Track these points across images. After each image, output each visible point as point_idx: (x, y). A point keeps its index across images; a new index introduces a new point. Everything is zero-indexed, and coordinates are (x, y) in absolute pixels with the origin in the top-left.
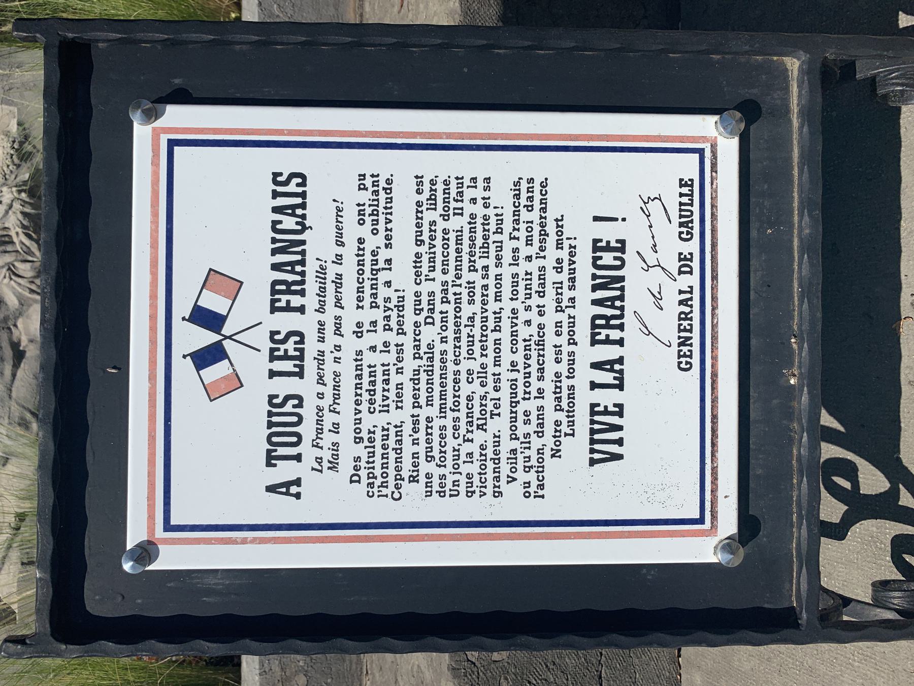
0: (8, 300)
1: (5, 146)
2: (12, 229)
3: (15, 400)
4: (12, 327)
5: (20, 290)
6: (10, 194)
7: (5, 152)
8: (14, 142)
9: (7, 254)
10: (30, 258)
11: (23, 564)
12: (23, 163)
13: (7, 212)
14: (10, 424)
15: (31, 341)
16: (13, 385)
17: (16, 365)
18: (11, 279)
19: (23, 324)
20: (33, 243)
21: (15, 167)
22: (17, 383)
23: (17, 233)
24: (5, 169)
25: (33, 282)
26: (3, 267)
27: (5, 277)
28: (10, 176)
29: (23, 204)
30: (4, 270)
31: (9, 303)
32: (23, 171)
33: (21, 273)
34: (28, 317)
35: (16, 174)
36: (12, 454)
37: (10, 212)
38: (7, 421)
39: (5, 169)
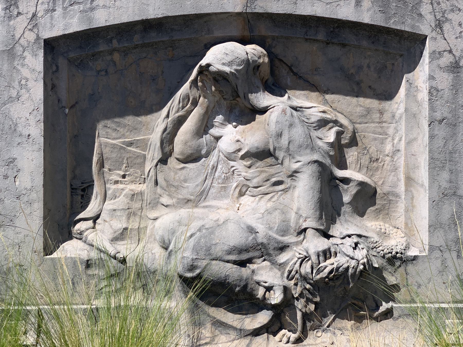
0: (283, 255)
1: (397, 247)
2: (336, 259)
3: (210, 263)
4: (264, 258)
5: (291, 264)
6: (362, 257)
7: (393, 248)
8: (402, 253)
9: (317, 257)
10: (314, 272)
11: (88, 261)
12: (385, 260)
13: (348, 256)
14: (193, 259)
15: (253, 271)
16: (220, 262)
17: (235, 262)
18: (299, 258)
19: (266, 266)
20: (326, 275)
21: (382, 255)
22: (222, 263)
23: (333, 264)
24: (381, 248)
25: (297, 272)
26: (307, 253)
27: (300, 254)
28: (375, 251)
29: (355, 267)
30: (305, 254)
31: (281, 256)
32: (380, 260)
33: (304, 265)
34: (271, 269)
35: (378, 255)
36: (170, 254)
37: (348, 258)
38: (195, 257)
39: (381, 248)
